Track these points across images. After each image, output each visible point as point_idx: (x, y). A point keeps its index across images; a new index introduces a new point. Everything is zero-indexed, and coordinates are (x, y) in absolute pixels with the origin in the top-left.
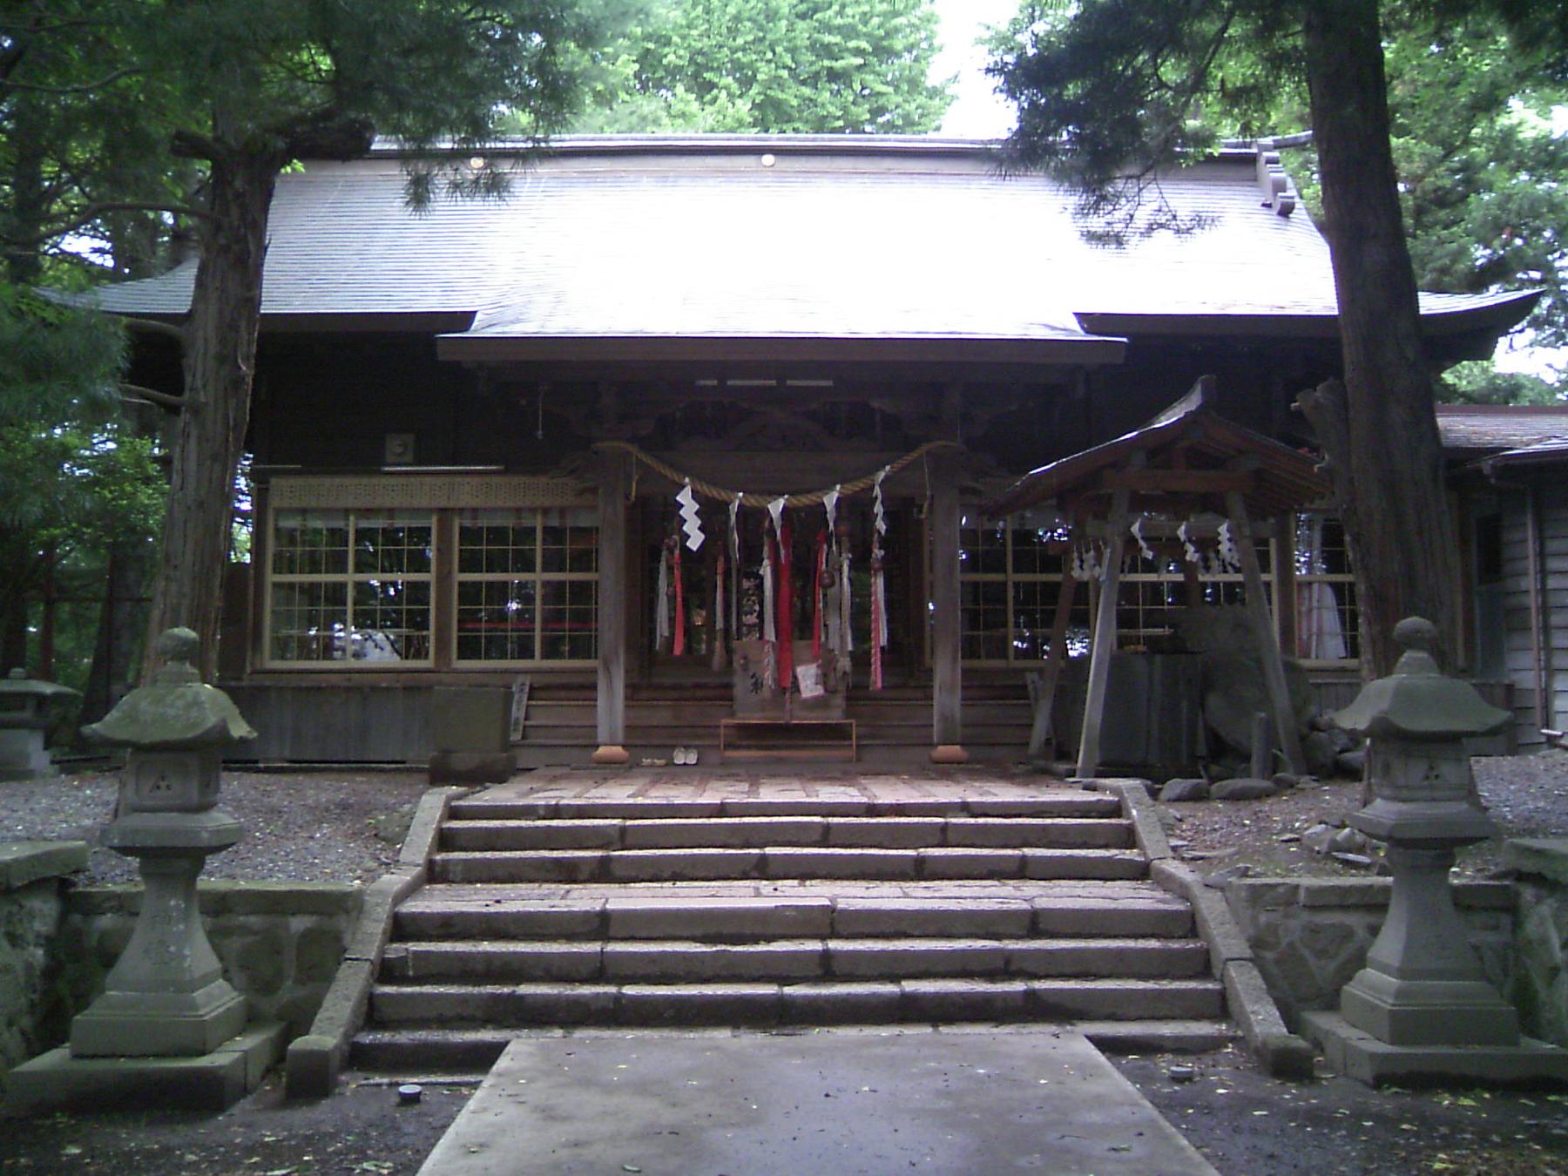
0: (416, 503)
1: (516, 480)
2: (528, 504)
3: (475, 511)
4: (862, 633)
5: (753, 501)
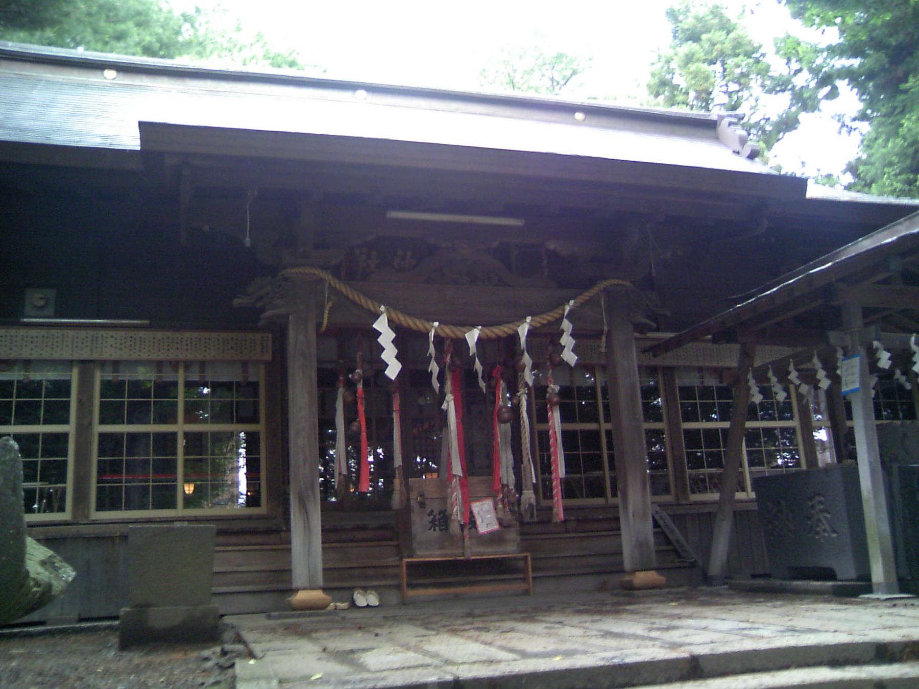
0: (56, 356)
1: (159, 335)
2: (171, 357)
3: (116, 364)
4: (545, 467)
5: (448, 331)
